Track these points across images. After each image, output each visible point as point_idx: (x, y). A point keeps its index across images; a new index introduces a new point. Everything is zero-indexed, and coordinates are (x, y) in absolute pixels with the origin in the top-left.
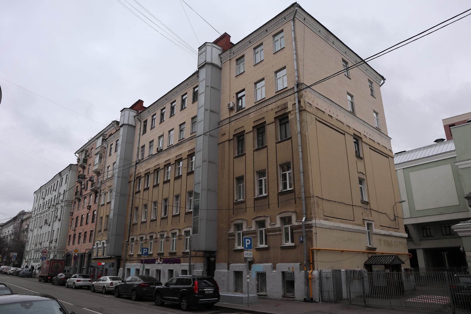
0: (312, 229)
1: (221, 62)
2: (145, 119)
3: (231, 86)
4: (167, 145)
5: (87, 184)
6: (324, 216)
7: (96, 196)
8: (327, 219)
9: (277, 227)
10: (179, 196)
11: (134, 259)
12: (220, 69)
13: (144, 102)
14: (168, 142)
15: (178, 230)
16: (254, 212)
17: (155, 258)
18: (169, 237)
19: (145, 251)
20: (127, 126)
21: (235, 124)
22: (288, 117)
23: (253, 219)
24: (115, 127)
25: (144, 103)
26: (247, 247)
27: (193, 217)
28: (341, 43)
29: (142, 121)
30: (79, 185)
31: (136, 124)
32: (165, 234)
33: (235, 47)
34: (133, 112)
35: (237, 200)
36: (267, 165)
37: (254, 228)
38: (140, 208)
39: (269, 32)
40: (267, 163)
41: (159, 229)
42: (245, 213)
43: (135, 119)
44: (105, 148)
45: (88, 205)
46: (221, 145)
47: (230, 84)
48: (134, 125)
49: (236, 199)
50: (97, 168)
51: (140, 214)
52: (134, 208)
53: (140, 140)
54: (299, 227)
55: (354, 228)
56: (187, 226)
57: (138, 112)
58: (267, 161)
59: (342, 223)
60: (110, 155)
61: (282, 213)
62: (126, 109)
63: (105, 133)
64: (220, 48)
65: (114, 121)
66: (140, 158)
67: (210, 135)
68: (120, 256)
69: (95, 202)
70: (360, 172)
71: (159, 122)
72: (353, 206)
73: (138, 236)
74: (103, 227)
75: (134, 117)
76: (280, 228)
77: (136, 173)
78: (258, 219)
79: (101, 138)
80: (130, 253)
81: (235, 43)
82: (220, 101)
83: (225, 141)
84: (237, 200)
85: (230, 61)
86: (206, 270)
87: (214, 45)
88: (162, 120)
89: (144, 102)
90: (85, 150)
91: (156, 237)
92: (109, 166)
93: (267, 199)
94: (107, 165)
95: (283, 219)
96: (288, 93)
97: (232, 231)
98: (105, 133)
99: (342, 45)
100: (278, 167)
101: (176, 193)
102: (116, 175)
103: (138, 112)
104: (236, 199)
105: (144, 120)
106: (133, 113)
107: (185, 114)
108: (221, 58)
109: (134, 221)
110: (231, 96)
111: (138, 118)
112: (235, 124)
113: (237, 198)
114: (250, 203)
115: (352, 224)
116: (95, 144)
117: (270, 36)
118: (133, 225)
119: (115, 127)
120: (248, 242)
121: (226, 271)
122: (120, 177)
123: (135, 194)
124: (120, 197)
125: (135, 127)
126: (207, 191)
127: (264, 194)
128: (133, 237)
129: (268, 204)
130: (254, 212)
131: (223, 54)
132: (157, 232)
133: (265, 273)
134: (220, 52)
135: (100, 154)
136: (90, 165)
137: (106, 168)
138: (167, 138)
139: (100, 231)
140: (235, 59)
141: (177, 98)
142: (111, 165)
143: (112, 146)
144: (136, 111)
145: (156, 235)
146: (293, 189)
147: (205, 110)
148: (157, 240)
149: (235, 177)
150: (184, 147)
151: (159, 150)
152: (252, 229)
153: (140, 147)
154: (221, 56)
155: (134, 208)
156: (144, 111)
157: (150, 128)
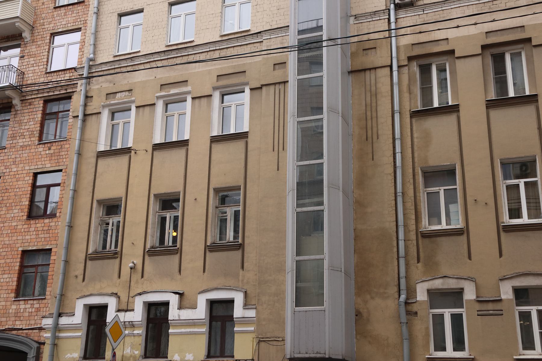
93: (464, 237)
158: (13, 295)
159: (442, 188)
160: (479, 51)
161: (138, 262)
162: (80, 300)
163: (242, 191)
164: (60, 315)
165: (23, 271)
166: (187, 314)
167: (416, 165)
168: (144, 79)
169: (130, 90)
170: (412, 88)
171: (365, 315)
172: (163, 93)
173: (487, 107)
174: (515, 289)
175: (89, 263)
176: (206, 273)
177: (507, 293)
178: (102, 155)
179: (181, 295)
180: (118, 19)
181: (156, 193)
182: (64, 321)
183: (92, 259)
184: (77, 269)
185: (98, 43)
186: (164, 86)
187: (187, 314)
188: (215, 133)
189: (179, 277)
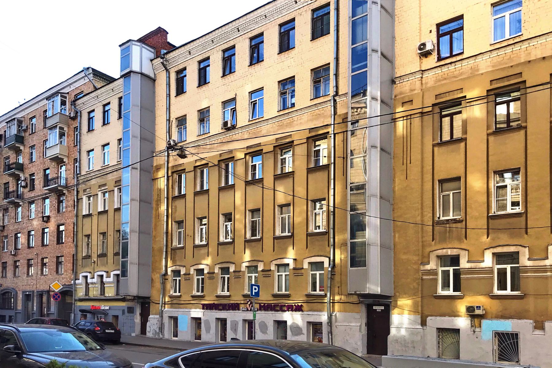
2: (181, 67)
11: (183, 302)
12: (154, 80)
13: (168, 33)
14: (248, 113)
17: (239, 302)
19: (255, 289)
20: (140, 75)
21: (436, 85)
25: (168, 35)
26: (254, 294)
27: (121, 260)
30: (10, 180)
31: (155, 74)
32: (259, 265)
33: (177, 51)
34: (148, 50)
38: (94, 237)
42: (465, 240)
43: (152, 64)
50: (58, 152)
51: (189, 232)
52: (173, 223)
56: (314, 255)
65: (88, 68)
67: (133, 168)
68: (149, 298)
74: (94, 249)
75: (152, 60)
77: (170, 165)
78: (499, 250)
80: (171, 293)
81: (177, 45)
84: (439, 218)
86: (366, 324)
88: (180, 90)
89: (168, 33)
90: (16, 120)
93: (184, 250)
95: (499, 258)
97: (432, 265)
100: (435, 183)
103: (157, 52)
105: (177, 69)
107: (292, 62)
109: (174, 244)
112: (436, 85)
113: (440, 215)
119: (90, 80)
120: (255, 289)
121: (420, 327)
123: (172, 200)
126: (380, 199)
129: (524, 227)
133: (517, 335)
136: (32, 147)
139: (88, 257)
140: (247, 36)
141: (268, 29)
149: (247, 209)
150: (295, 122)
154: (153, 62)
155: (173, 223)
158: (72, 272)
159: (452, 192)
160: (305, 141)
161: (95, 260)
162: (192, 267)
163: (463, 180)
164: (76, 280)
165: (248, 248)
166: (108, 280)
167: (490, 168)
168: (94, 183)
169: (90, 188)
170: (174, 186)
171: (154, 280)
172: (100, 190)
173: (275, 179)
174: (459, 258)
175: (83, 260)
176: (307, 249)
177: (192, 272)
178: (84, 216)
179: (107, 272)
180: (118, 142)
181: (441, 178)
182: (77, 282)
183: (84, 259)
184: (80, 262)
185: (81, 166)
186: (405, 104)
187: (108, 280)
188: (116, 207)
189: (526, 236)
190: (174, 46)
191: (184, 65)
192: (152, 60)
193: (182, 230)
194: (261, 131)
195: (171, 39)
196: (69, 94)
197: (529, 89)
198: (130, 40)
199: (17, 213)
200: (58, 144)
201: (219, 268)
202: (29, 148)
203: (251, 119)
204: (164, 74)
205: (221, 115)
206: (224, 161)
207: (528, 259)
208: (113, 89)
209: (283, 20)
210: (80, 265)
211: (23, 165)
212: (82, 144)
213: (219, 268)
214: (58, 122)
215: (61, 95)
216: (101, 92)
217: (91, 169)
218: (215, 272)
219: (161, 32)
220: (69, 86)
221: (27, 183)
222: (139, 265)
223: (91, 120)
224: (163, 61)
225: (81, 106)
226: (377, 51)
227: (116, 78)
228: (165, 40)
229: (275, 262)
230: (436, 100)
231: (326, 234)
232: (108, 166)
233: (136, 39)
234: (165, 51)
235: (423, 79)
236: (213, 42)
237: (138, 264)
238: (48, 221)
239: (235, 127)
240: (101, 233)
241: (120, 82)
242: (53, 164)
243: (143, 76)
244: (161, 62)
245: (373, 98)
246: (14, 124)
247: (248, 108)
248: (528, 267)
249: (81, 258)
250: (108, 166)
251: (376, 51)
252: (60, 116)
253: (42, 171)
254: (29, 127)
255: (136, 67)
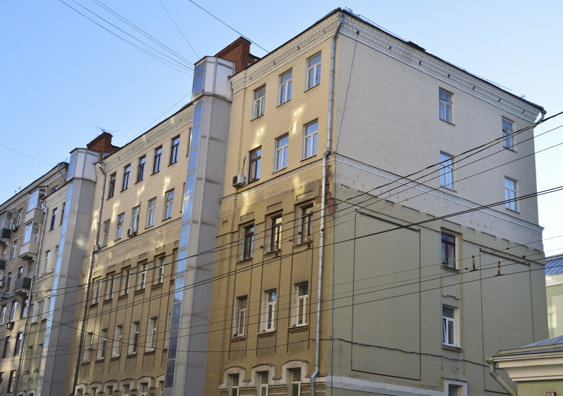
0: (324, 391)
1: (231, 91)
2: (113, 171)
3: (243, 136)
4: (144, 225)
5: (8, 279)
6: (352, 370)
7: (24, 305)
8: (357, 376)
9: (281, 384)
10: (157, 319)
13: (112, 136)
14: (145, 221)
15: (150, 379)
16: (256, 357)
18: (136, 390)
20: (81, 180)
22: (313, 205)
23: (253, 368)
24: (62, 175)
25: (112, 138)
28: (437, 61)
29: (108, 174)
31: (97, 177)
33: (120, 151)
35: (236, 335)
36: (278, 281)
37: (283, 381)
39: (302, 51)
40: (278, 278)
41: (122, 375)
42: (245, 357)
43: (95, 168)
44: (44, 214)
45: (8, 321)
46: (220, 238)
47: (242, 133)
48: (93, 179)
49: (234, 333)
53: (103, 209)
54: (308, 385)
55: (416, 393)
57: (102, 155)
58: (279, 275)
59: (387, 382)
60: (52, 228)
61: (290, 362)
62: (80, 150)
63: (45, 184)
64: (231, 64)
65: (61, 163)
66: (101, 243)
69: (21, 317)
70: (447, 295)
71: (135, 181)
72: (422, 355)
73: (89, 385)
76: (286, 385)
79: (37, 193)
81: (120, 146)
82: (226, 161)
83: (226, 234)
85: (245, 91)
87: (220, 60)
88: (140, 178)
89: (112, 136)
90: (7, 212)
91: (102, 390)
92: (49, 251)
94: (45, 249)
96: (315, 167)
98: (45, 184)
99: (441, 63)
101: (152, 315)
102: (58, 270)
103: (101, 155)
104: (234, 333)
106: (93, 158)
108: (231, 83)
110: (242, 155)
111: (101, 168)
113: (237, 332)
114: (252, 342)
115: (414, 386)
116: (26, 204)
117: (303, 58)
118: (84, 365)
119: (62, 175)
122: (64, 276)
123: (90, 308)
124: (62, 313)
125: (96, 183)
127: (304, 324)
128: (81, 387)
130: (256, 357)
131: (235, 77)
132: (103, 382)
134: (231, 73)
135: (34, 223)
137: (44, 254)
138: (146, 214)
140: (153, 147)
142: (53, 250)
143: (56, 211)
144: (97, 154)
145: (118, 386)
146: (308, 324)
147: (197, 179)
148: (155, 391)
149: (236, 296)
151: (131, 234)
152: (251, 384)
153: (102, 223)
154: (232, 79)
156: (111, 157)
157: (120, 189)
189: (275, 354)
190: (119, 148)
191: (128, 162)
192: (230, 77)
193: (305, 297)
194: (149, 240)
195: (254, 51)
196: (49, 187)
197: (119, 272)
198: (206, 57)
199: (12, 310)
200: (29, 242)
201: (107, 387)
202: (13, 243)
203: (147, 227)
204: (102, 177)
205: (130, 221)
206: (111, 274)
207: (273, 378)
208: (181, 120)
209: (177, 133)
210: (20, 383)
211: (5, 262)
212: (44, 244)
213: (123, 385)
214: (32, 219)
215: (40, 189)
216: (62, 190)
217: (281, 167)
218: (156, 387)
219: (106, 137)
220: (48, 179)
221: (4, 283)
222: (52, 383)
223: (158, 157)
224: (101, 166)
225: (48, 203)
226: (201, 179)
227: (261, 58)
228: (108, 143)
229: (140, 381)
230: (139, 258)
231: (153, 354)
232: (284, 172)
233: (213, 56)
234: (250, 64)
235: (237, 201)
236: (299, 49)
237: (51, 382)
238: (12, 327)
239: (136, 234)
240: (266, 291)
241: (191, 109)
242: (25, 263)
243: (84, 181)
244: (100, 167)
245: (194, 222)
246: (4, 218)
247: (146, 216)
248: (273, 387)
249: (229, 340)
250: (312, 160)
251: (201, 179)
252: (35, 210)
253: (17, 270)
254: (16, 220)
255: (208, 89)
